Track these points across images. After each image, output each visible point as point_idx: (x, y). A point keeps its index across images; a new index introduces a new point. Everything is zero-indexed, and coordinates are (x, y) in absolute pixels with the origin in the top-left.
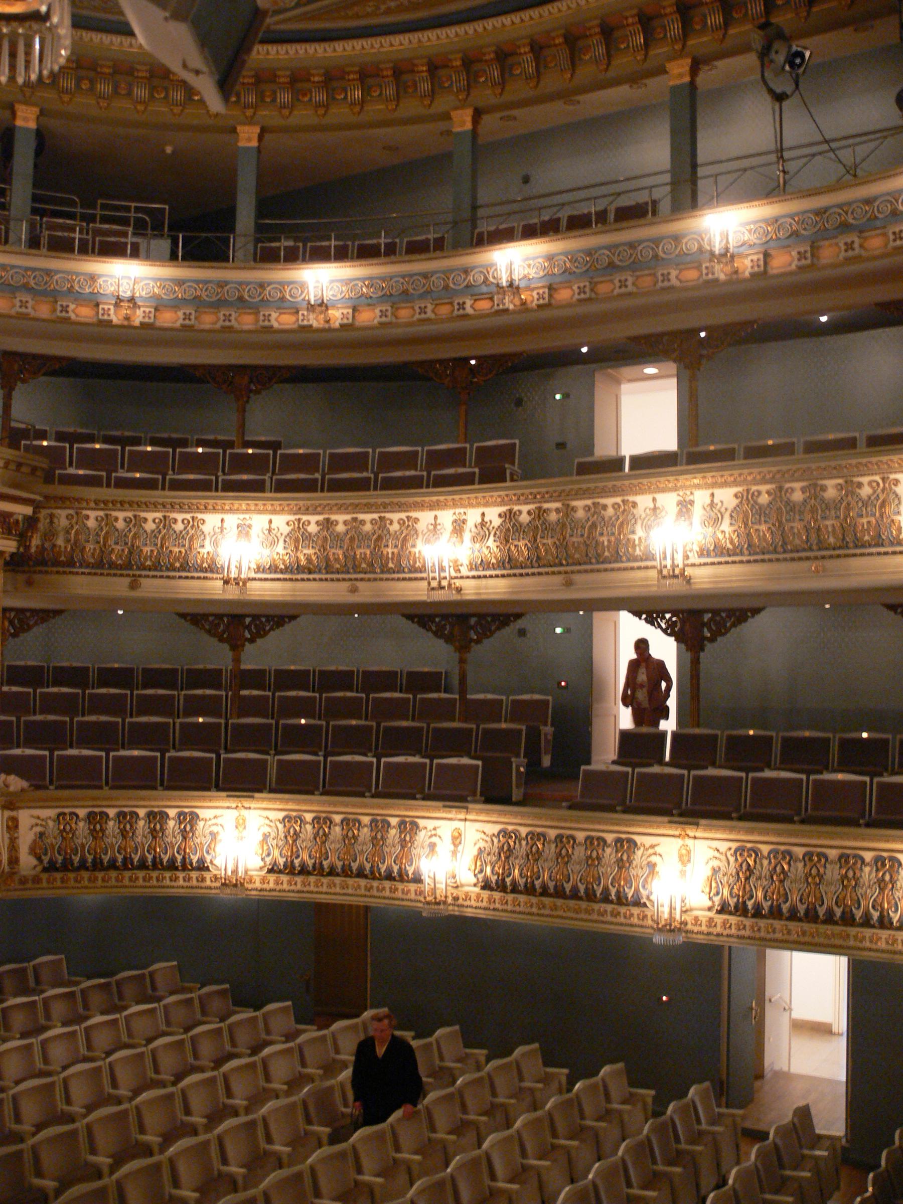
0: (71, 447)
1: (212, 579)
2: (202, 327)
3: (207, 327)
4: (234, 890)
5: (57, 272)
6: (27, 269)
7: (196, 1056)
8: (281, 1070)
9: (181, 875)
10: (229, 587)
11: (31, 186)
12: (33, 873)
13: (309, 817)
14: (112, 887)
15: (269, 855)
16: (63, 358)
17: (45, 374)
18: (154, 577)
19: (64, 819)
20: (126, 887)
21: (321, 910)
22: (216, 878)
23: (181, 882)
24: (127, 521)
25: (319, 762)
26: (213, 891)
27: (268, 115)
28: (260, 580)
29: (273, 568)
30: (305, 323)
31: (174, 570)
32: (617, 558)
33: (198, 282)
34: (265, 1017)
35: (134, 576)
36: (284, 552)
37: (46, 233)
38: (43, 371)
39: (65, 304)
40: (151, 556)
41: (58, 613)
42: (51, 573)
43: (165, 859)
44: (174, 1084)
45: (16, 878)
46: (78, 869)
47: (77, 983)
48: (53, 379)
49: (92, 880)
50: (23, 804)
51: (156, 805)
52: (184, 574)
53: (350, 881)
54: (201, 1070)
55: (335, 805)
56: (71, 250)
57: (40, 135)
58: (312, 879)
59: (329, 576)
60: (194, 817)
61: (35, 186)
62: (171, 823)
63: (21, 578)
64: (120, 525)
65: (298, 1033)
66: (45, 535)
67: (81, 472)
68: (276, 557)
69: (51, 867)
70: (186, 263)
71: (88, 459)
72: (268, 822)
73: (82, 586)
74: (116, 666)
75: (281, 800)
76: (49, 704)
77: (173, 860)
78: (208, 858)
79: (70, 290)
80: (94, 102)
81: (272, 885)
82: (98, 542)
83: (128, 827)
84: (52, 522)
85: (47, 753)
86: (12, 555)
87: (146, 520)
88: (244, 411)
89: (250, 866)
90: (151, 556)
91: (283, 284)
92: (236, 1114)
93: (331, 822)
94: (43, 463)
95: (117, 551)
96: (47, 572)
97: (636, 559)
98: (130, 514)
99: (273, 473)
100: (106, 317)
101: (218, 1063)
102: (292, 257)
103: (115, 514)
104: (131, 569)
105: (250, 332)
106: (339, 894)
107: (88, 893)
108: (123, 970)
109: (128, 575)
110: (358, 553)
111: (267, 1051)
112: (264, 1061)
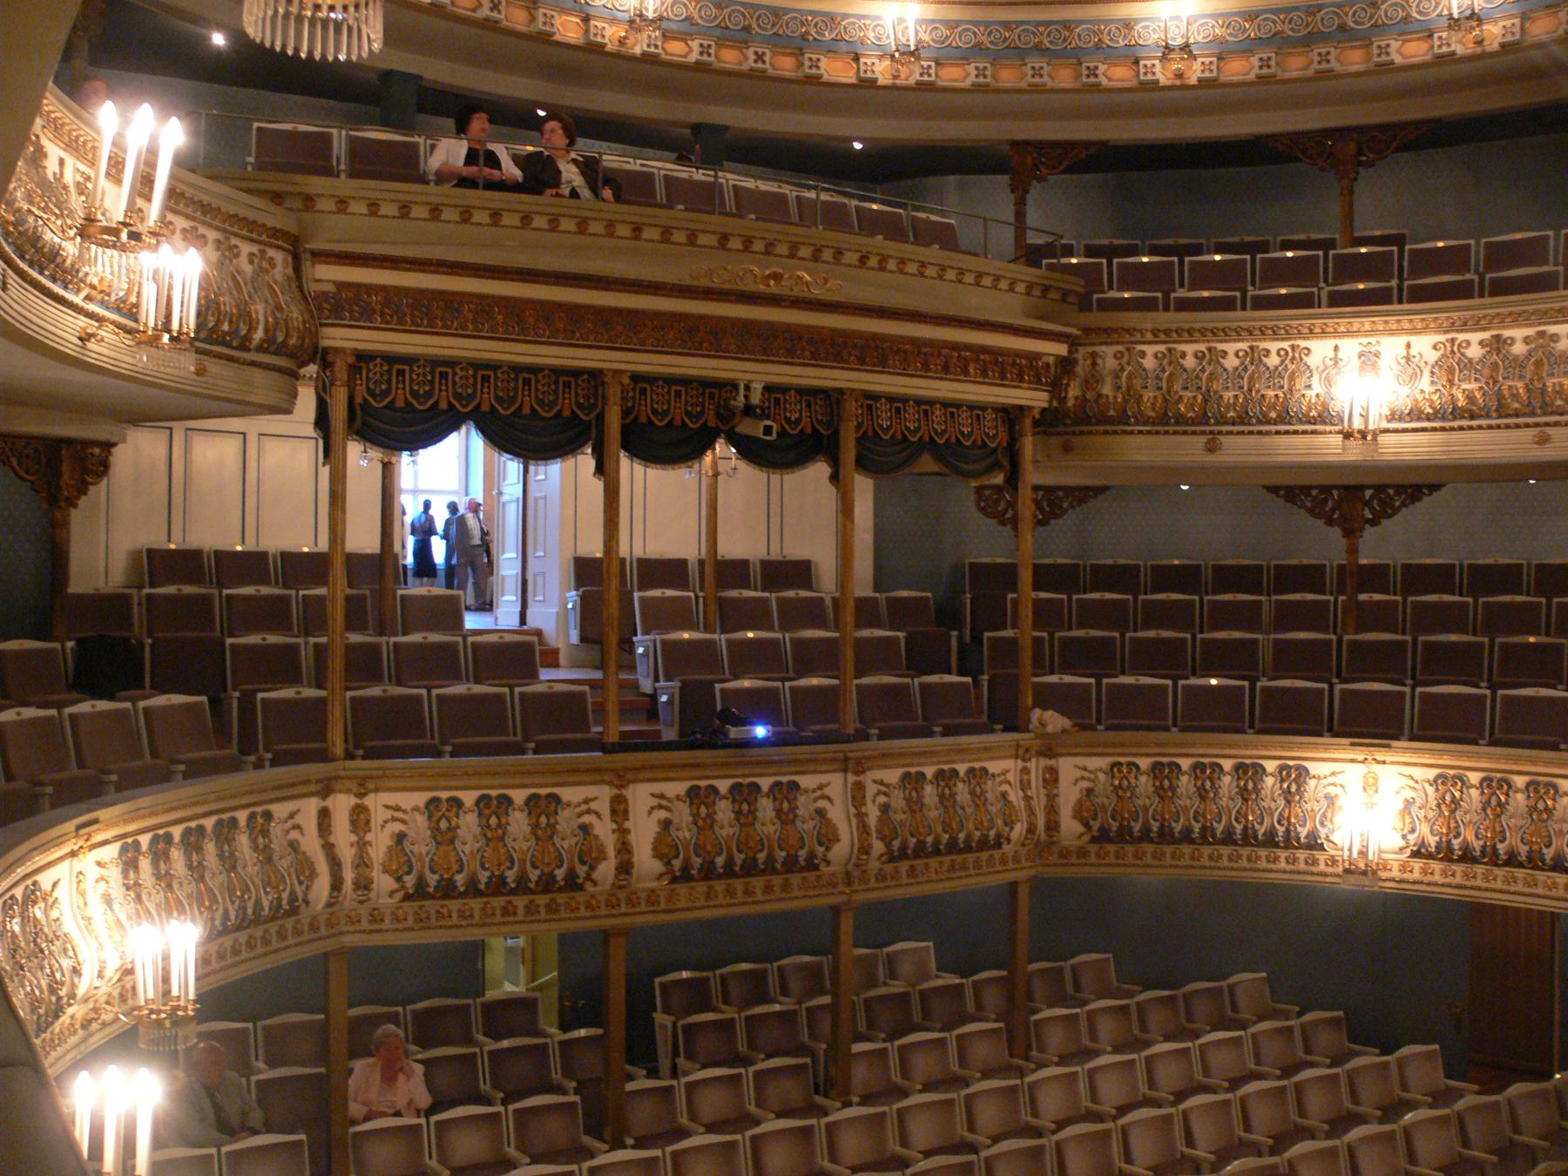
0: (1110, 264)
1: (1324, 433)
2: (1287, 75)
3: (1295, 74)
5: (1081, 22)
9: (1283, 854)
10: (1351, 442)
12: (1078, 843)
13: (1474, 777)
15: (1413, 831)
19: (1120, 771)
21: (1479, 911)
22: (1333, 861)
23: (1283, 865)
24: (1199, 356)
26: (1329, 879)
28: (1396, 431)
29: (1416, 414)
30: (1445, 49)
31: (1268, 423)
34: (1401, 1064)
35: (1211, 432)
36: (1432, 389)
39: (1092, 65)
40: (1235, 404)
41: (1102, 490)
43: (1261, 830)
45: (1055, 849)
46: (1140, 840)
51: (1248, 754)
52: (1283, 428)
53: (1541, 876)
55: (1516, 761)
58: (1479, 869)
60: (1303, 773)
62: (1269, 781)
63: (1055, 441)
64: (1190, 362)
65: (1460, 1094)
66: (1086, 381)
68: (1420, 397)
69: (1103, 837)
71: (1134, 277)
72: (1412, 783)
73: (1140, 450)
76: (1090, 616)
77: (1271, 833)
78: (1323, 832)
79: (1098, 46)
81: (1416, 875)
82: (1160, 388)
84: (1094, 364)
86: (1044, 410)
88: (1351, 193)
89: (1385, 847)
90: (1235, 404)
93: (1510, 787)
96: (1090, 433)
98: (1202, 347)
99: (1401, 278)
100: (1150, 77)
104: (1207, 424)
105: (1358, 74)
107: (1149, 872)
108: (983, 970)
109: (1203, 433)
110: (1549, 383)
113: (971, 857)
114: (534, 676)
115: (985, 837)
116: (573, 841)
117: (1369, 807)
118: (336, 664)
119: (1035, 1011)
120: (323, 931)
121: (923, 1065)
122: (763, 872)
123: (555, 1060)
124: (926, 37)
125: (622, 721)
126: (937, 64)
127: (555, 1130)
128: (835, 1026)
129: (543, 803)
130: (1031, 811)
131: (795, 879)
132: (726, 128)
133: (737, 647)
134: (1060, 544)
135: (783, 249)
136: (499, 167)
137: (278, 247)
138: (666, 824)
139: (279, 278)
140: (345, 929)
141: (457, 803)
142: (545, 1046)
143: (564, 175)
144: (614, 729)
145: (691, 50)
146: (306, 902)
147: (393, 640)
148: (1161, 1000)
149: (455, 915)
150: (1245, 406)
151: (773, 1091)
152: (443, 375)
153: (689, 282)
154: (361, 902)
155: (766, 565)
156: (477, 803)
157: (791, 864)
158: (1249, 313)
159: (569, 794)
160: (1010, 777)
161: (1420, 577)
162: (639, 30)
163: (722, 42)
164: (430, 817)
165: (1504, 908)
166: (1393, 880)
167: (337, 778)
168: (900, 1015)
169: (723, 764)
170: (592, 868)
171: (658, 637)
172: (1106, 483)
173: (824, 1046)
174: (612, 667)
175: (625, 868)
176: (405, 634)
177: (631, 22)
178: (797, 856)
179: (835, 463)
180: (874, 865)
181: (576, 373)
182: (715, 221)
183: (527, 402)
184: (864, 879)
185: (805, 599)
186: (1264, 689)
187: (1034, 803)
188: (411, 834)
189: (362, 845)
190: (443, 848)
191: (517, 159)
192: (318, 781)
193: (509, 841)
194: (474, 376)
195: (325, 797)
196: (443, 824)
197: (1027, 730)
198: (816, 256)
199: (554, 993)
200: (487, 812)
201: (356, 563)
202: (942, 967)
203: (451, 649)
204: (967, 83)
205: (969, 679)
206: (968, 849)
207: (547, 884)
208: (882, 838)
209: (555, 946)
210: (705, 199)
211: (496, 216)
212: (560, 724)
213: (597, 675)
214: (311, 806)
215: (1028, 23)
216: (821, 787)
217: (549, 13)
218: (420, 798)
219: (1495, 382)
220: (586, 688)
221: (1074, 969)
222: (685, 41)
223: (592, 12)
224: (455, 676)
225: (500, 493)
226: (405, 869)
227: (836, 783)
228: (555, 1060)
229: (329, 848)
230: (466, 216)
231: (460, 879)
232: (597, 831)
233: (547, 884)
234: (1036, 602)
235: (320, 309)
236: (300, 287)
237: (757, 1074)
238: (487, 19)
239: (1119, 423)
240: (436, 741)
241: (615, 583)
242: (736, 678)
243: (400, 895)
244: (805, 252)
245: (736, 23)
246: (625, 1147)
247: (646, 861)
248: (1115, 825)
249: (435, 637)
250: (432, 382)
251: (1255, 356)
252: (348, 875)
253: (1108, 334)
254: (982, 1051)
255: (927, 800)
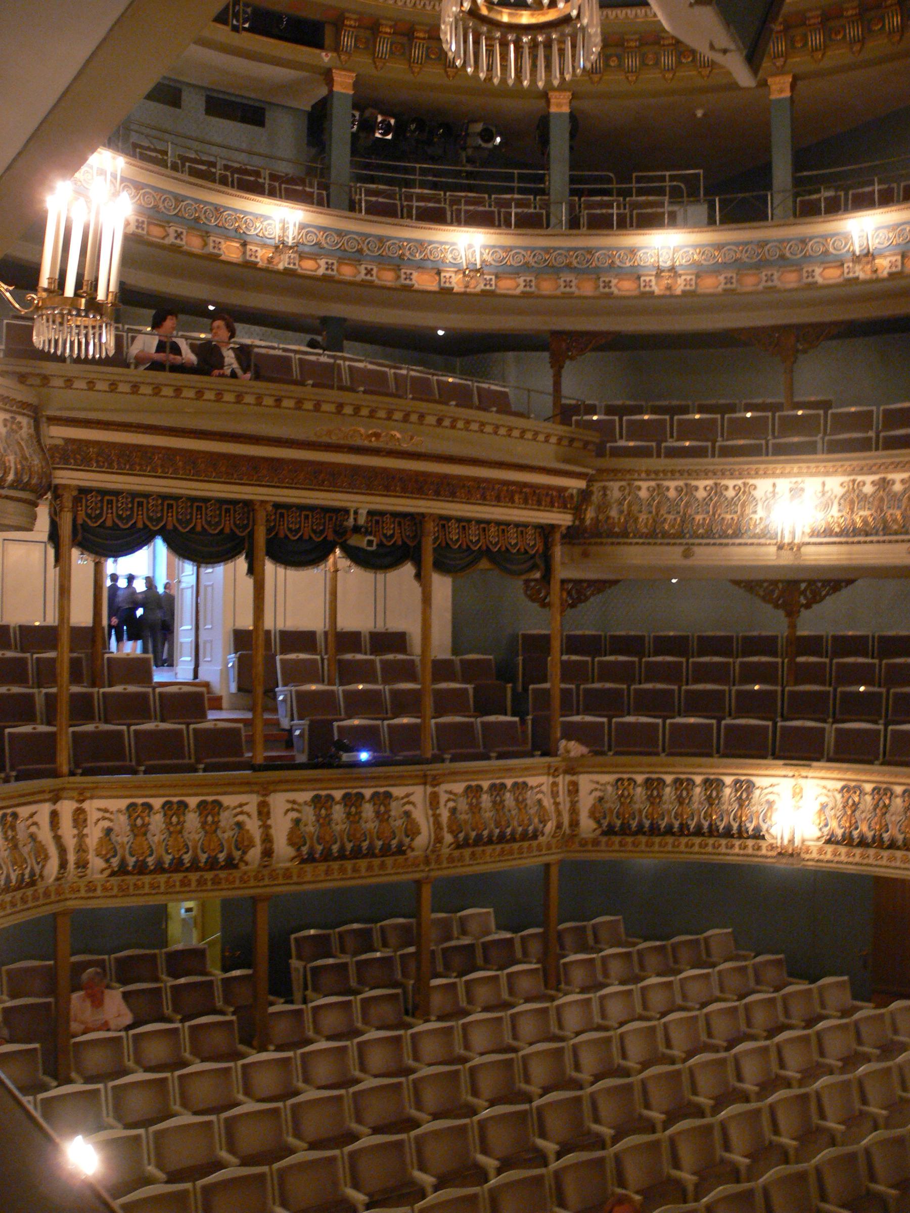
0: (621, 420)
1: (765, 545)
4: (791, 860)
5: (598, 249)
6: (570, 249)
7: (749, 1024)
8: (836, 1047)
9: (737, 843)
10: (783, 552)
11: (567, 168)
12: (592, 835)
13: (868, 787)
14: (669, 852)
15: (826, 825)
16: (608, 333)
17: (593, 350)
18: (708, 544)
20: (682, 852)
21: (880, 882)
22: (772, 847)
23: (737, 850)
24: (679, 490)
25: (879, 731)
26: (769, 860)
27: (800, 62)
28: (815, 544)
29: (828, 532)
30: (851, 275)
32: (737, 534)
33: (737, 244)
35: (687, 544)
37: (585, 212)
38: (590, 347)
39: (607, 280)
40: (703, 524)
41: (615, 582)
42: (606, 544)
44: (727, 1049)
45: (577, 840)
46: (636, 833)
47: (634, 944)
48: (600, 353)
49: (649, 845)
50: (581, 769)
51: (712, 772)
54: (753, 1038)
56: (610, 226)
57: (573, 117)
58: (871, 852)
59: (887, 538)
60: (751, 786)
61: (572, 168)
62: (727, 791)
63: (578, 550)
64: (672, 494)
65: (857, 1009)
67: (631, 444)
69: (610, 831)
70: (726, 226)
71: (638, 430)
72: (825, 791)
73: (636, 556)
74: (671, 634)
75: (839, 769)
77: (728, 828)
78: (764, 827)
80: (623, 77)
81: (829, 856)
82: (650, 512)
83: (684, 793)
84: (605, 495)
85: (605, 720)
86: (569, 527)
87: (697, 488)
88: (792, 371)
89: (807, 836)
90: (703, 524)
91: (825, 237)
92: (789, 1086)
94: (594, 437)
95: (670, 521)
96: (601, 543)
97: (755, 536)
99: (825, 433)
100: (647, 289)
101: (772, 1033)
102: (835, 208)
103: (666, 483)
105: (751, 293)
106: (899, 868)
107: (647, 857)
109: (681, 544)
111: (821, 1025)
112: (818, 1034)
113: (516, 846)
114: (203, 716)
115: (525, 832)
116: (231, 833)
117: (797, 809)
118: (64, 708)
119: (564, 956)
120: (53, 898)
121: (483, 994)
122: (365, 856)
123: (218, 992)
124: (488, 258)
125: (266, 749)
126: (497, 277)
127: (218, 1039)
128: (418, 968)
129: (210, 807)
130: (559, 813)
131: (389, 861)
132: (345, 320)
133: (351, 696)
134: (587, 621)
135: (382, 414)
136: (180, 354)
137: (24, 414)
138: (297, 822)
139: (25, 436)
140: (69, 896)
141: (148, 807)
142: (211, 982)
143: (226, 360)
144: (261, 755)
145: (319, 267)
146: (41, 876)
147: (102, 690)
148: (656, 948)
149: (147, 886)
150: (710, 526)
151: (374, 1012)
152: (140, 504)
153: (314, 439)
154: (81, 877)
155: (374, 636)
156: (163, 806)
157: (386, 851)
158: (717, 460)
159: (228, 800)
160: (544, 788)
161: (847, 645)
162: (282, 252)
163: (341, 261)
164: (130, 816)
165: (896, 880)
166: (812, 860)
167: (64, 789)
168: (467, 959)
169: (338, 779)
170: (245, 853)
171: (294, 689)
172: (619, 577)
173: (412, 982)
174: (259, 709)
175: (268, 853)
176: (110, 686)
177: (277, 247)
178: (390, 845)
179: (418, 564)
180: (445, 851)
181: (234, 502)
182: (335, 395)
183: (199, 523)
184: (438, 860)
185: (402, 661)
186: (727, 726)
187: (561, 807)
188: (116, 828)
189: (81, 837)
190: (139, 839)
191: (193, 348)
192: (50, 792)
193: (185, 834)
194: (162, 504)
195: (55, 803)
196: (139, 822)
197: (556, 755)
198: (406, 419)
199: (218, 948)
200: (170, 813)
201: (78, 633)
202: (499, 927)
203: (142, 698)
204: (518, 291)
205: (516, 719)
206: (513, 839)
207: (212, 865)
208: (451, 831)
209: (218, 909)
210: (325, 377)
211: (178, 390)
212: (222, 752)
213: (249, 715)
214: (45, 809)
215: (559, 248)
216: (408, 795)
217: (218, 240)
218: (123, 803)
219: (882, 511)
220: (241, 725)
221: (594, 926)
222: (315, 259)
223: (248, 240)
224: (146, 715)
225: (179, 582)
226: (112, 853)
227: (419, 793)
228: (218, 992)
229: (58, 839)
230: (157, 390)
231: (151, 861)
232: (248, 827)
233: (212, 865)
234: (563, 663)
235: (52, 457)
236: (39, 441)
237: (362, 1000)
238: (173, 245)
239: (623, 537)
240: (134, 763)
241: (261, 652)
242: (350, 718)
243: (108, 872)
244: (398, 416)
245: (351, 247)
246: (267, 1050)
247: (282, 848)
248: (619, 823)
249: (132, 689)
250: (132, 509)
251: (717, 490)
252: (72, 858)
253: (615, 473)
254: (525, 985)
255: (483, 805)
